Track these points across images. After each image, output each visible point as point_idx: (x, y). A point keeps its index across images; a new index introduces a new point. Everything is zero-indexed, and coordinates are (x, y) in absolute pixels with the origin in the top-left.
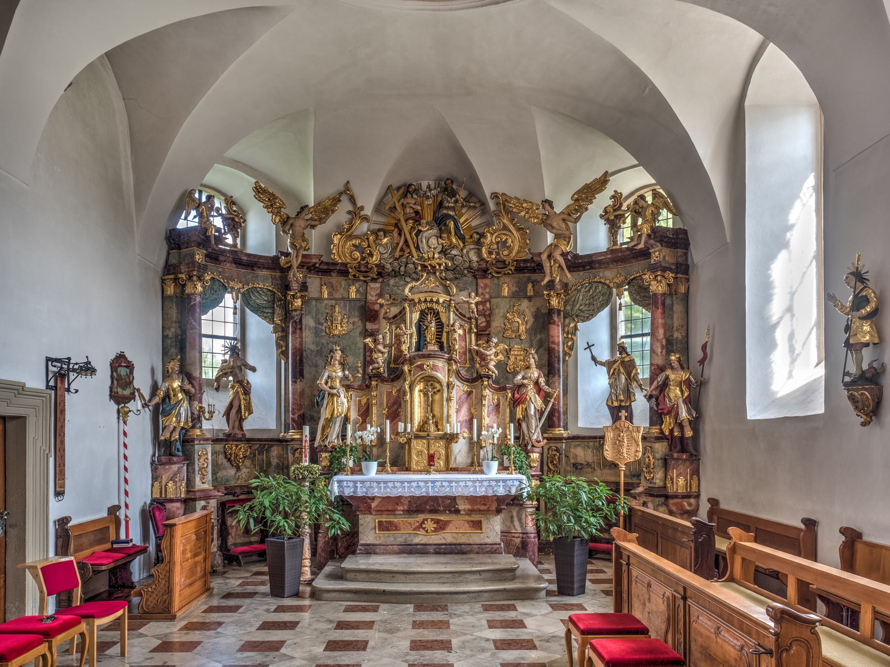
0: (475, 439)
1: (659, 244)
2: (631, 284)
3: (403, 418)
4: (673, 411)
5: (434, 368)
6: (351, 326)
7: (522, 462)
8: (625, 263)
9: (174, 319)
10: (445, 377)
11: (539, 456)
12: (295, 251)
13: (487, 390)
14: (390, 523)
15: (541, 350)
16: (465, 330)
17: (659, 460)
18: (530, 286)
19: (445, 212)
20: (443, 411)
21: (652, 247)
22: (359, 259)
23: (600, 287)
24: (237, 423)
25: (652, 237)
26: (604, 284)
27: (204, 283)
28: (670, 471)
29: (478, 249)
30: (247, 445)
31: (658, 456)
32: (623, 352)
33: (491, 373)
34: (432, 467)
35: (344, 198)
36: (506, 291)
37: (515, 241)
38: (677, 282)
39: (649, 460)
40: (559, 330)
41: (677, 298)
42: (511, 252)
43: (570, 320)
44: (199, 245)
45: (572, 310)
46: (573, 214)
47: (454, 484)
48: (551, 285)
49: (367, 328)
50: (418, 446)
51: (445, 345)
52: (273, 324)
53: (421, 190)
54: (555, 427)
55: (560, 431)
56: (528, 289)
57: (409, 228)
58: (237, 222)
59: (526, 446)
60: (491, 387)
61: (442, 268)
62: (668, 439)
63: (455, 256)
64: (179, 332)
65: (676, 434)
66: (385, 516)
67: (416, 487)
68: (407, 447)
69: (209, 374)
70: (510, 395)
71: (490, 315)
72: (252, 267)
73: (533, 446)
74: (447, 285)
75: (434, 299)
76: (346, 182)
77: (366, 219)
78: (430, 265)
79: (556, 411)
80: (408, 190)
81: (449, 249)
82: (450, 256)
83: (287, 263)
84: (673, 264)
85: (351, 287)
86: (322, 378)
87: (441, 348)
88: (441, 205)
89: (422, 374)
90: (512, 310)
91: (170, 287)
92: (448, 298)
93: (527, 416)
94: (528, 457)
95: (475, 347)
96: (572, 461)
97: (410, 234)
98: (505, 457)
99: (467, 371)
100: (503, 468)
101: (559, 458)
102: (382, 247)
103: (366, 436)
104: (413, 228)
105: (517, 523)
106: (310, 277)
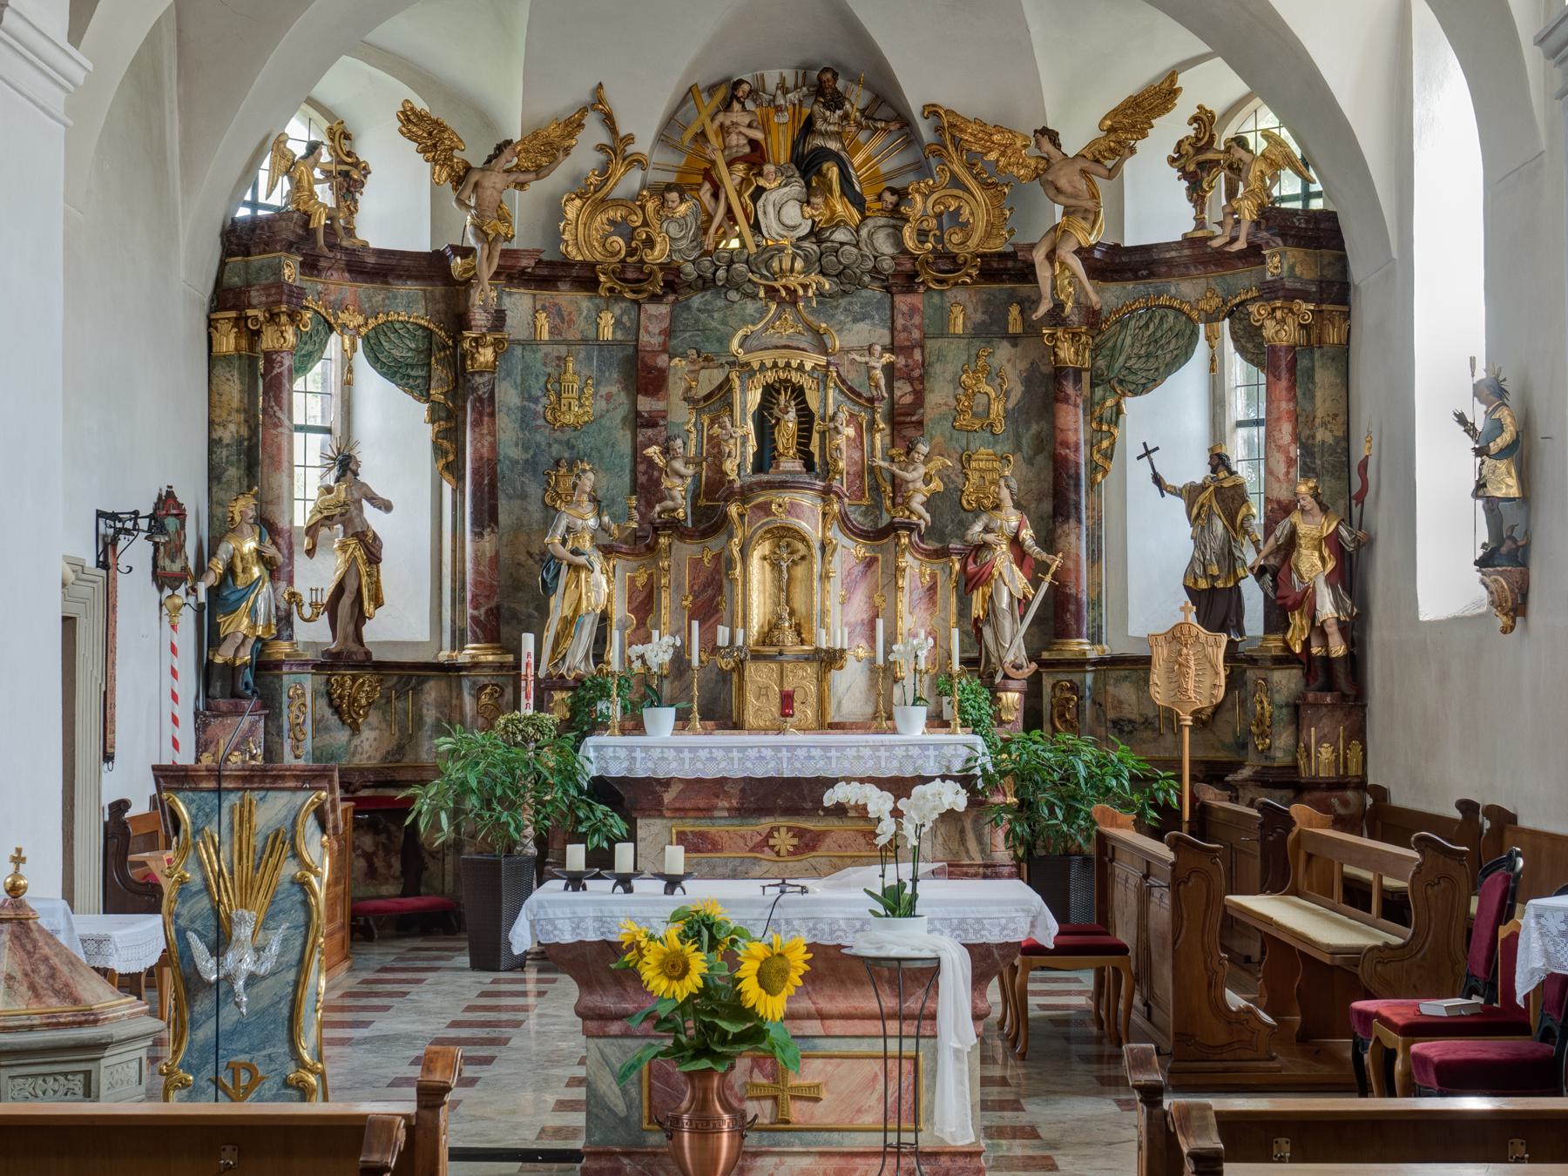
0: (880, 661)
1: (1279, 241)
2: (1237, 315)
3: (726, 615)
4: (1306, 602)
5: (793, 509)
6: (603, 404)
7: (980, 709)
8: (1222, 267)
9: (235, 404)
10: (816, 529)
11: (1019, 699)
12: (486, 246)
13: (908, 556)
14: (702, 835)
15: (1041, 460)
16: (861, 425)
17: (1281, 707)
18: (1014, 311)
19: (819, 142)
20: (812, 602)
21: (1268, 245)
22: (623, 252)
23: (1171, 319)
24: (351, 628)
25: (1263, 226)
26: (1180, 311)
27: (298, 326)
28: (1305, 732)
29: (894, 227)
30: (376, 677)
31: (1280, 698)
32: (1221, 468)
33: (915, 518)
34: (788, 719)
35: (592, 121)
36: (960, 321)
37: (977, 209)
38: (1323, 320)
39: (1262, 708)
40: (1076, 415)
41: (1322, 355)
42: (968, 237)
43: (1105, 390)
44: (290, 247)
45: (1109, 367)
46: (1105, 157)
47: (833, 753)
48: (1056, 316)
49: (640, 408)
50: (759, 676)
51: (817, 459)
52: (427, 401)
53: (764, 91)
54: (1070, 637)
55: (1080, 646)
56: (1011, 318)
57: (738, 180)
58: (355, 181)
59: (992, 676)
60: (917, 549)
61: (810, 293)
62: (1300, 662)
63: (842, 244)
64: (245, 432)
65: (1315, 650)
66: (691, 821)
67: (756, 758)
68: (735, 677)
69: (301, 516)
70: (957, 566)
71: (921, 379)
72: (385, 276)
73: (1006, 677)
74: (821, 331)
75: (794, 364)
76: (595, 84)
77: (638, 162)
78: (786, 288)
79: (1072, 600)
80: (731, 92)
81: (827, 229)
82: (829, 244)
83: (466, 271)
84: (1312, 282)
85: (602, 315)
86: (554, 531)
87: (809, 465)
88: (808, 127)
89: (767, 523)
90: (973, 367)
91: (227, 337)
92: (823, 360)
93: (994, 611)
94: (995, 700)
95: (882, 464)
96: (1111, 714)
97: (740, 194)
98: (946, 699)
99: (865, 514)
100: (937, 721)
101: (1077, 705)
102: (674, 224)
103: (653, 655)
104: (745, 181)
105: (972, 845)
106: (510, 294)
